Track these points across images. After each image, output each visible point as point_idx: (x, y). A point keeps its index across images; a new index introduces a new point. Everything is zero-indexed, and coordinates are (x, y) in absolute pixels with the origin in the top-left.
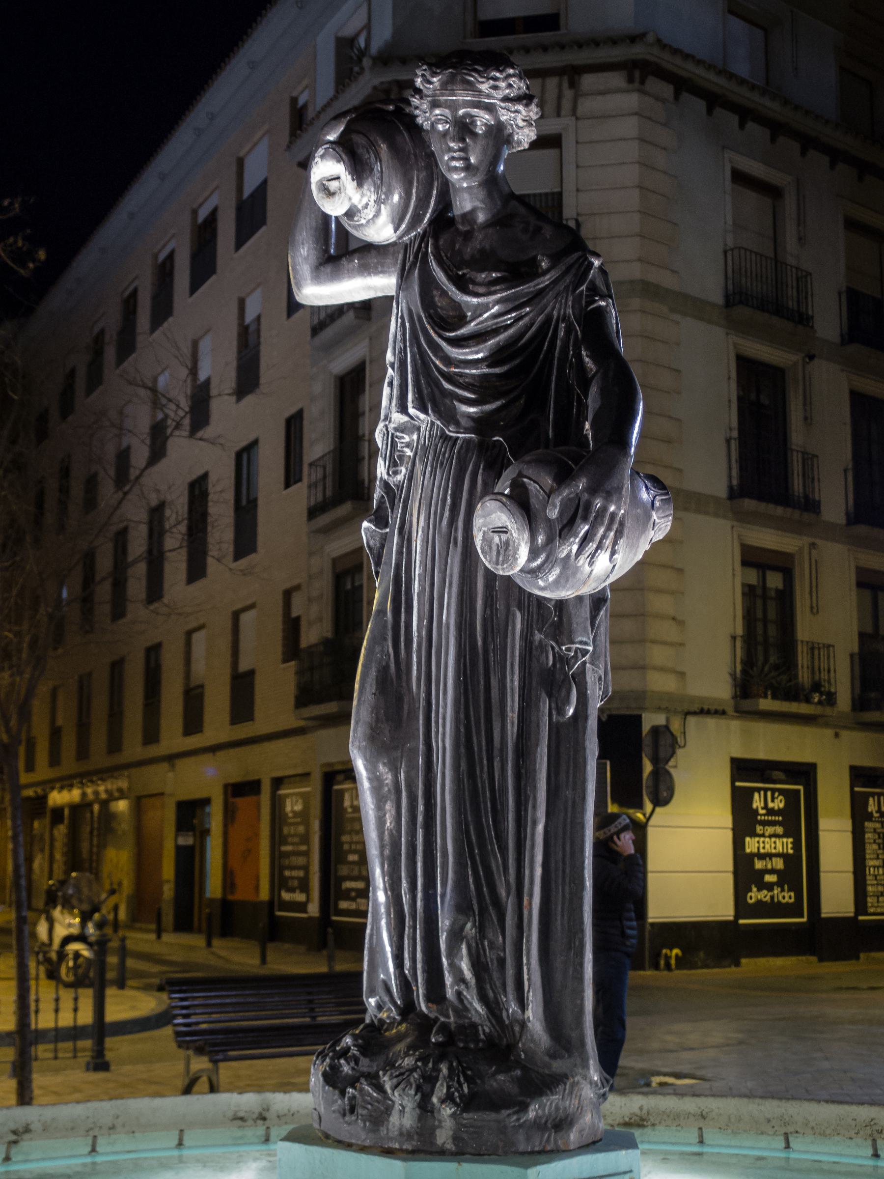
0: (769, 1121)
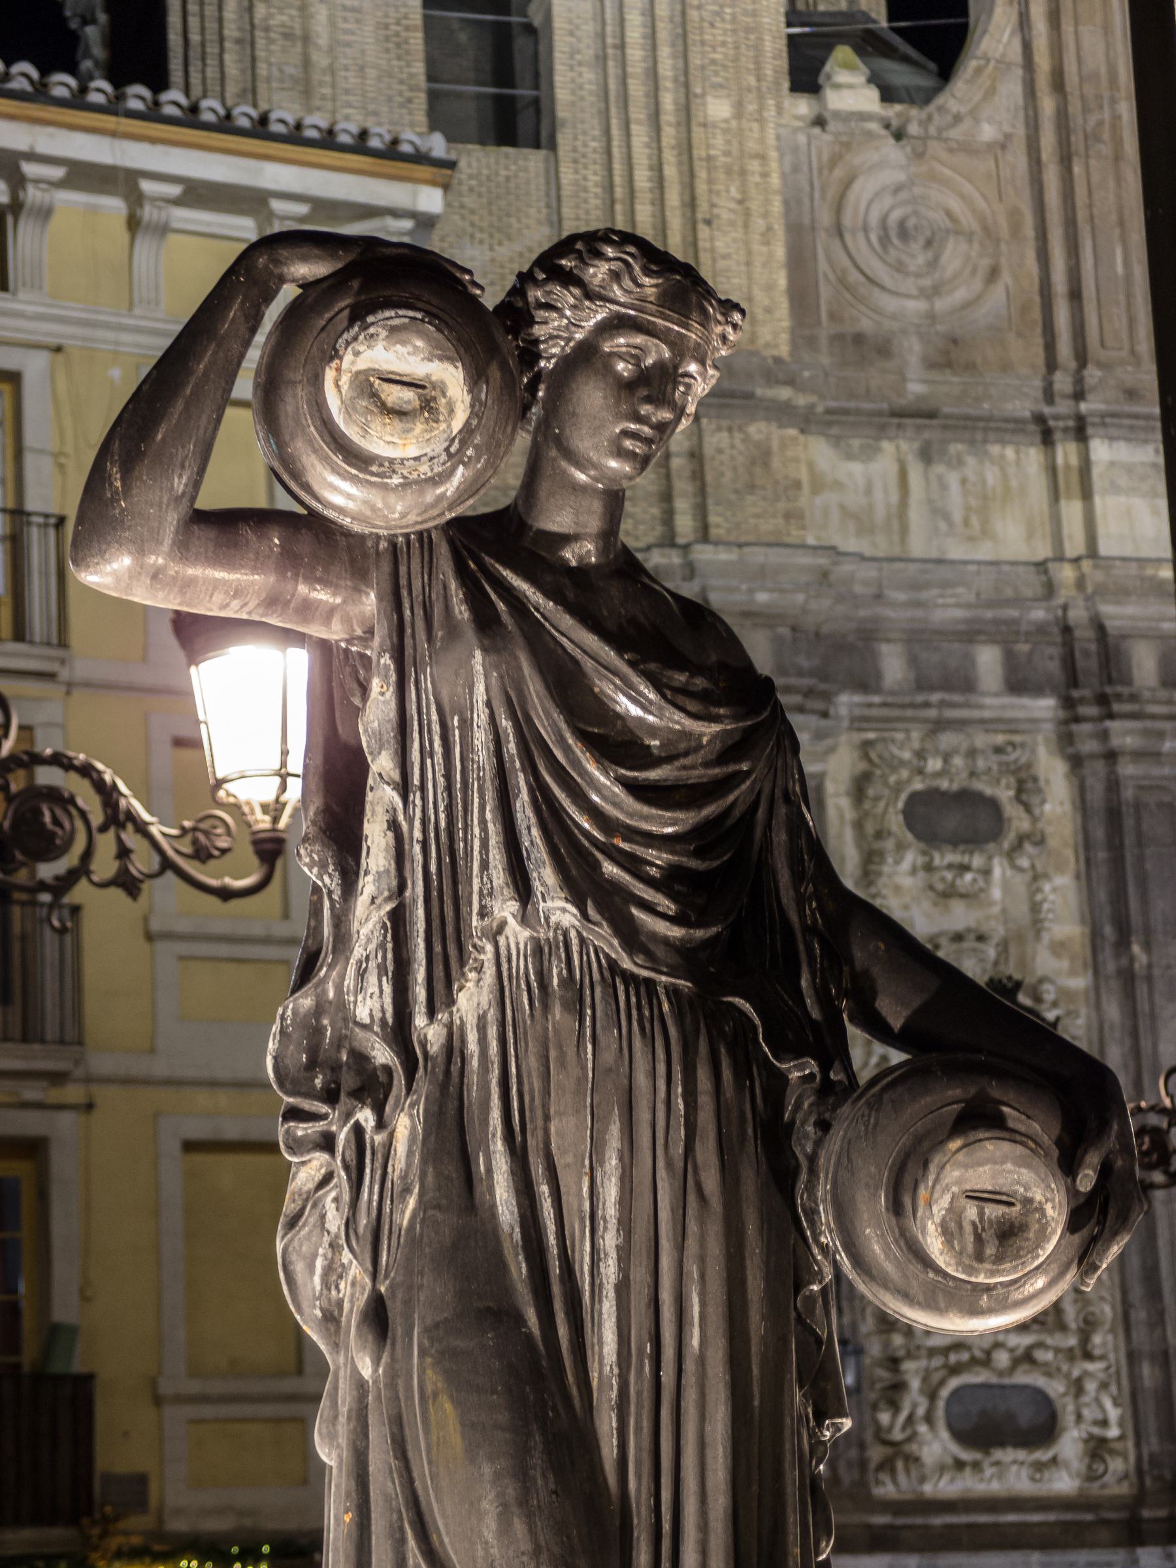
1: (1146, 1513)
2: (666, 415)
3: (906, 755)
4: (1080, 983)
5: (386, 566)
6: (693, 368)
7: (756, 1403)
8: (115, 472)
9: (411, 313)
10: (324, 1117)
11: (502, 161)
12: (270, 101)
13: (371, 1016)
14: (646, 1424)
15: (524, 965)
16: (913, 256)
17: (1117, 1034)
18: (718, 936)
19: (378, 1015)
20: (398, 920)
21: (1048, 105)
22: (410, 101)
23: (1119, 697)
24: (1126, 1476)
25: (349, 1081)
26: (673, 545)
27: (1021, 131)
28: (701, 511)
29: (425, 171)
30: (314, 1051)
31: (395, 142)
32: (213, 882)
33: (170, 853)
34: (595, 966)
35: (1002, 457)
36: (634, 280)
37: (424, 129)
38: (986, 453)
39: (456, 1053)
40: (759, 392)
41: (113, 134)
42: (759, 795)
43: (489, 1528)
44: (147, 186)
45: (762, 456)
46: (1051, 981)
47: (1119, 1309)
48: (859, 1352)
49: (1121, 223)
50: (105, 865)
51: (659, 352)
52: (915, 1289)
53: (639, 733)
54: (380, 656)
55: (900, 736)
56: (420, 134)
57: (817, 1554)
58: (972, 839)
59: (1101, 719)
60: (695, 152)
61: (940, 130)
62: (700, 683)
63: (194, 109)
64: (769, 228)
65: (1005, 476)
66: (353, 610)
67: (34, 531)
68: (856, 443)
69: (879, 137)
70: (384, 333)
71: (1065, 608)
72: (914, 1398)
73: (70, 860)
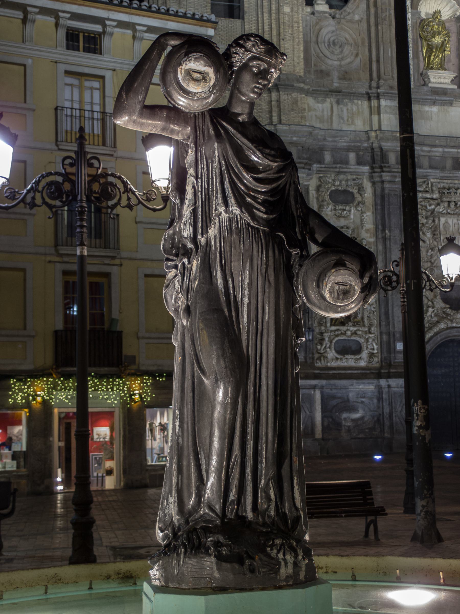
0: (3, 584)
1: (382, 371)
2: (266, 82)
3: (330, 181)
4: (372, 240)
5: (193, 120)
6: (273, 70)
7: (281, 333)
8: (124, 94)
9: (200, 54)
10: (175, 260)
11: (230, 22)
12: (170, 5)
13: (187, 235)
14: (254, 338)
15: (226, 223)
16: (336, 50)
17: (381, 253)
18: (275, 218)
19: (189, 235)
20: (194, 211)
21: (372, 10)
22: (206, 6)
23: (385, 167)
24: (378, 362)
25: (181, 251)
26: (272, 125)
27: (365, 17)
28: (279, 116)
29: (210, 24)
30: (173, 244)
31: (202, 16)
32: (152, 207)
33: (141, 199)
34: (244, 224)
35: (358, 103)
36: (258, 47)
37: (210, 13)
38: (353, 102)
39: (209, 245)
40: (295, 85)
41: (129, 13)
42: (287, 182)
43: (214, 362)
44: (138, 27)
45: (296, 102)
46: (365, 239)
47: (378, 321)
48: (313, 331)
49: (390, 42)
50: (124, 202)
51: (264, 66)
52: (323, 307)
53: (257, 165)
54: (191, 144)
55: (329, 175)
56: (209, 15)
57: (296, 370)
58: (346, 203)
59: (380, 172)
60: (280, 21)
61: (344, 16)
62: (273, 152)
63: (150, 7)
64: (299, 42)
65: (358, 109)
66: (184, 132)
67: (108, 117)
68: (320, 99)
69: (328, 18)
70: (193, 59)
71: (372, 143)
72: (326, 342)
73: (115, 201)
